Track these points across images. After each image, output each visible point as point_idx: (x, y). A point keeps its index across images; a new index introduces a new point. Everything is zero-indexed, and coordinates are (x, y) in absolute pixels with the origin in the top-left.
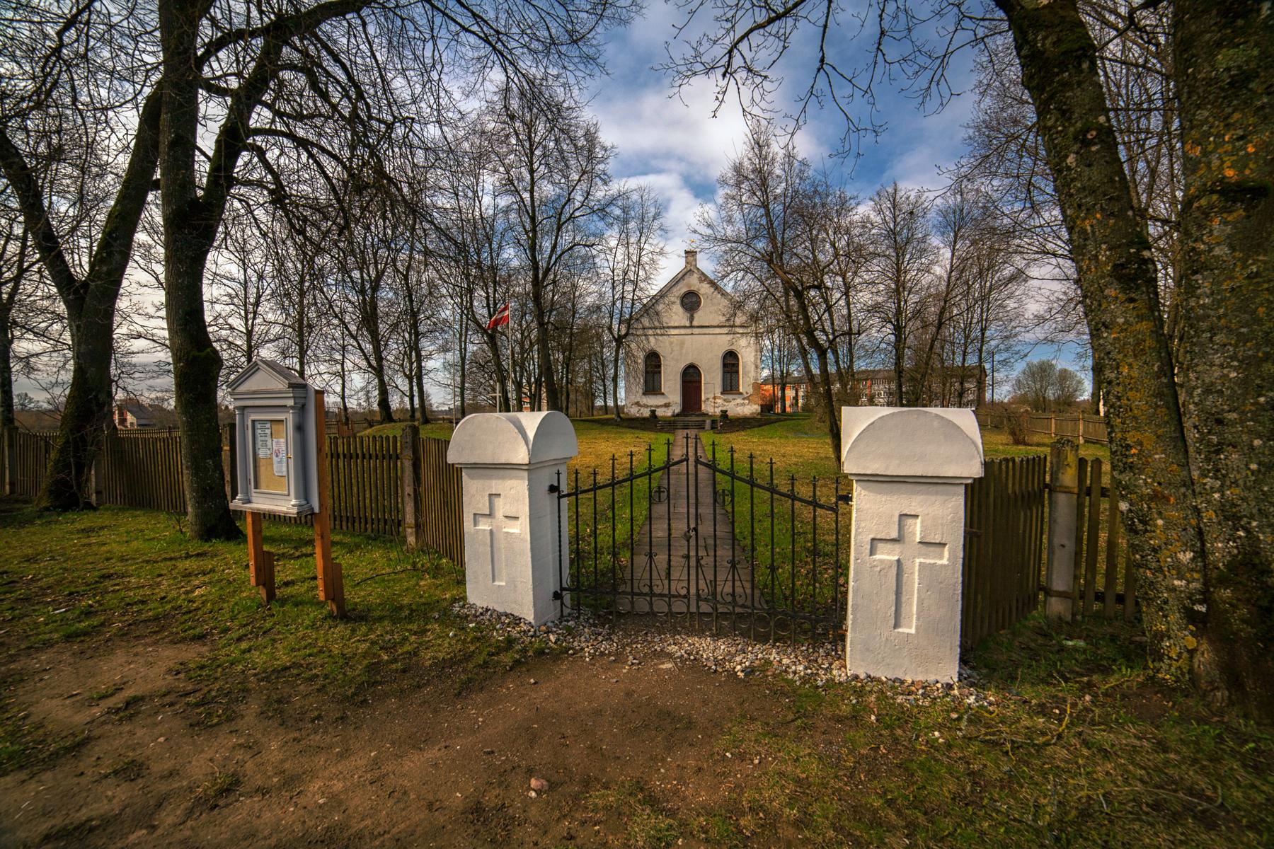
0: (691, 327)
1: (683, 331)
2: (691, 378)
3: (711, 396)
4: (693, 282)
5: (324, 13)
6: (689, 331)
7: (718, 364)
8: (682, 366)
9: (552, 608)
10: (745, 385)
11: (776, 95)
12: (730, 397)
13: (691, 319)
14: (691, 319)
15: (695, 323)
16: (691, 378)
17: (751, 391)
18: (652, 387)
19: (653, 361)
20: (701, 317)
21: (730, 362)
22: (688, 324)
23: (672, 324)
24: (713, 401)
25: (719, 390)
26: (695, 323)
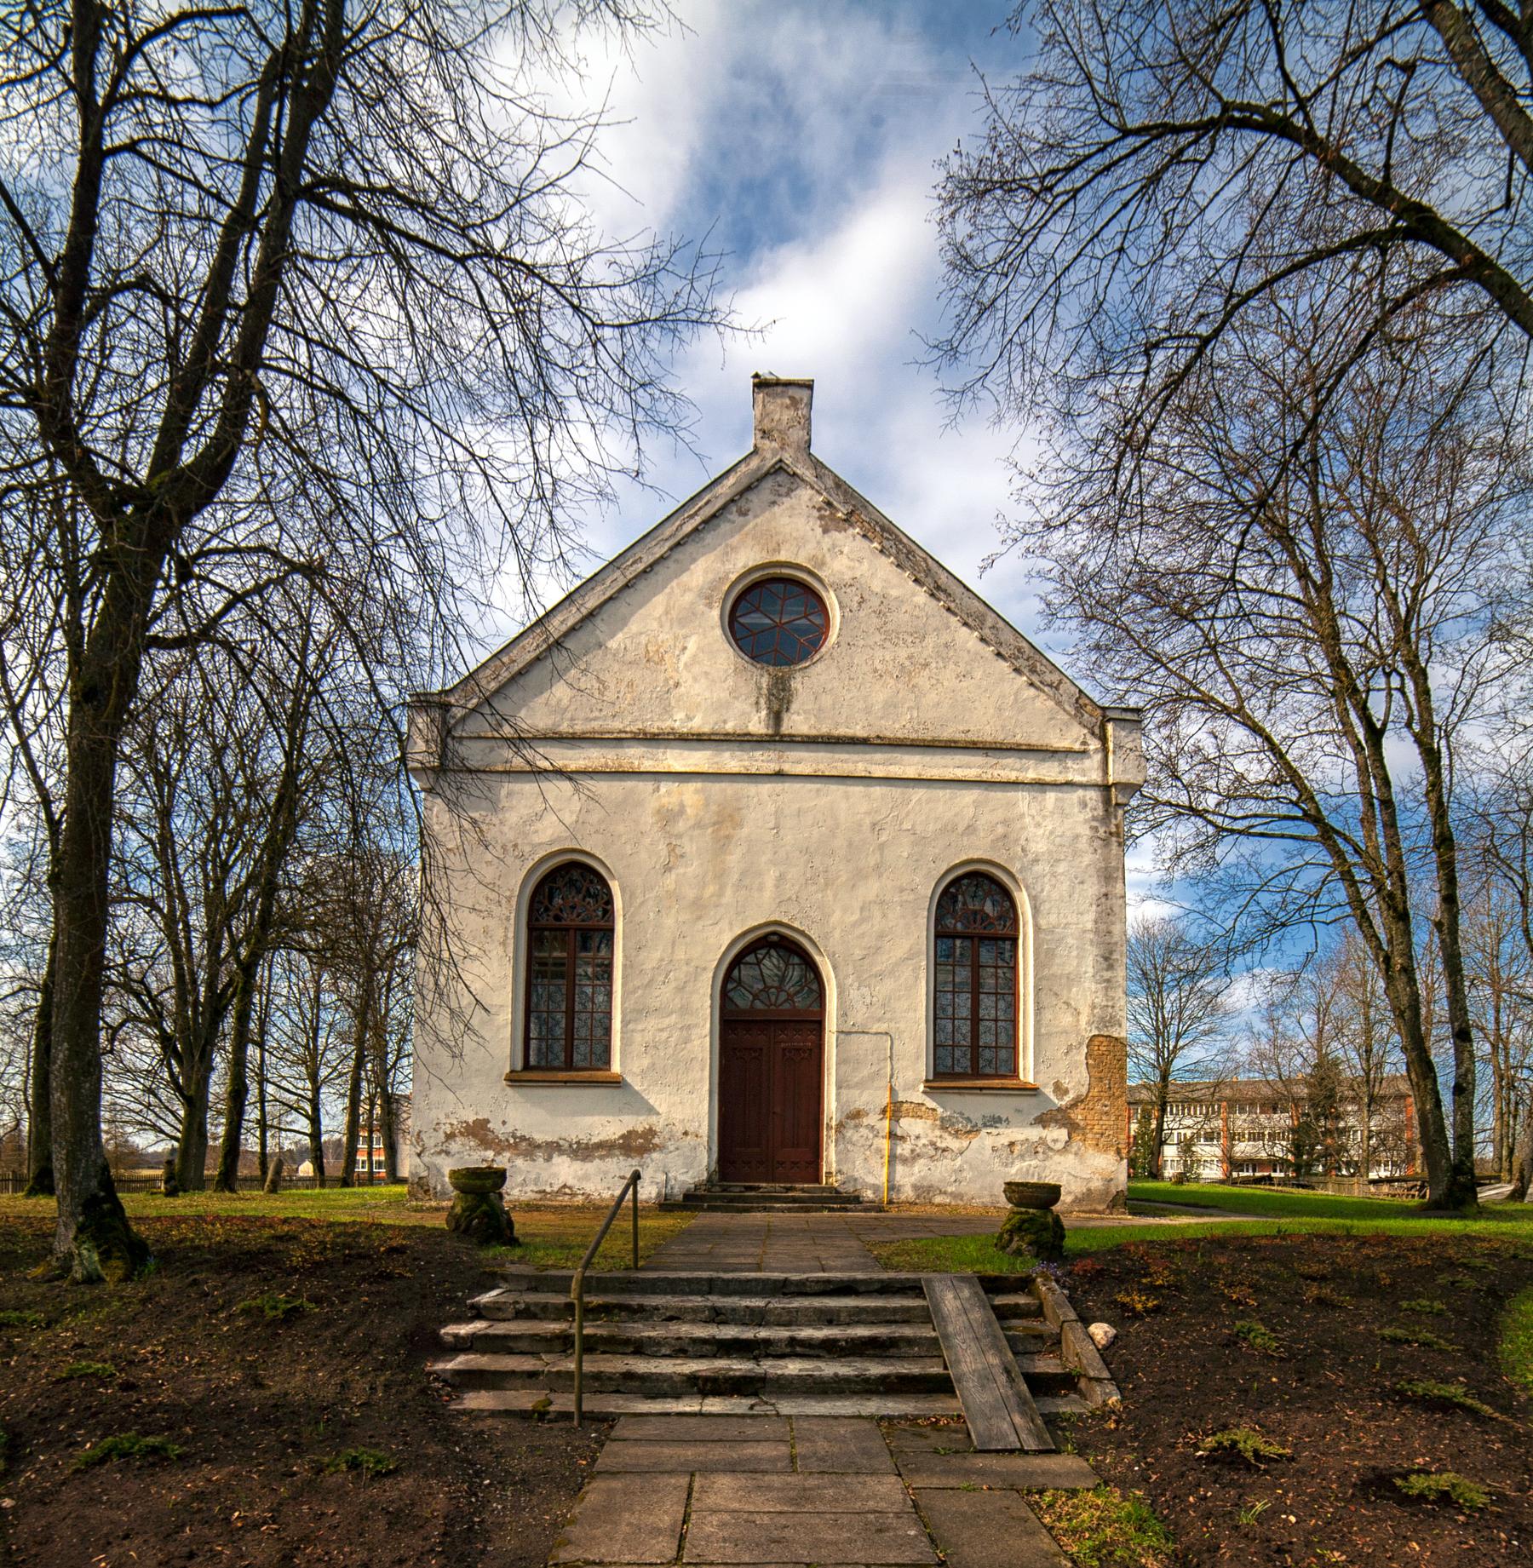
0: (777, 739)
1: (731, 761)
2: (769, 1018)
3: (874, 1098)
4: (791, 532)
5: (6, 685)
6: (763, 760)
7: (912, 936)
8: (717, 939)
9: (747, 689)
10: (1052, 1038)
11: (1004, 83)
12: (977, 1106)
13: (779, 701)
14: (779, 701)
15: (797, 722)
16: (769, 1018)
17: (1077, 1079)
18: (562, 1038)
19: (568, 914)
20: (825, 693)
21: (974, 918)
22: (757, 724)
23: (678, 722)
24: (898, 1137)
25: (914, 1067)
26: (797, 722)
